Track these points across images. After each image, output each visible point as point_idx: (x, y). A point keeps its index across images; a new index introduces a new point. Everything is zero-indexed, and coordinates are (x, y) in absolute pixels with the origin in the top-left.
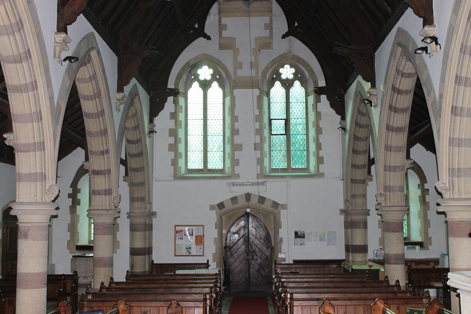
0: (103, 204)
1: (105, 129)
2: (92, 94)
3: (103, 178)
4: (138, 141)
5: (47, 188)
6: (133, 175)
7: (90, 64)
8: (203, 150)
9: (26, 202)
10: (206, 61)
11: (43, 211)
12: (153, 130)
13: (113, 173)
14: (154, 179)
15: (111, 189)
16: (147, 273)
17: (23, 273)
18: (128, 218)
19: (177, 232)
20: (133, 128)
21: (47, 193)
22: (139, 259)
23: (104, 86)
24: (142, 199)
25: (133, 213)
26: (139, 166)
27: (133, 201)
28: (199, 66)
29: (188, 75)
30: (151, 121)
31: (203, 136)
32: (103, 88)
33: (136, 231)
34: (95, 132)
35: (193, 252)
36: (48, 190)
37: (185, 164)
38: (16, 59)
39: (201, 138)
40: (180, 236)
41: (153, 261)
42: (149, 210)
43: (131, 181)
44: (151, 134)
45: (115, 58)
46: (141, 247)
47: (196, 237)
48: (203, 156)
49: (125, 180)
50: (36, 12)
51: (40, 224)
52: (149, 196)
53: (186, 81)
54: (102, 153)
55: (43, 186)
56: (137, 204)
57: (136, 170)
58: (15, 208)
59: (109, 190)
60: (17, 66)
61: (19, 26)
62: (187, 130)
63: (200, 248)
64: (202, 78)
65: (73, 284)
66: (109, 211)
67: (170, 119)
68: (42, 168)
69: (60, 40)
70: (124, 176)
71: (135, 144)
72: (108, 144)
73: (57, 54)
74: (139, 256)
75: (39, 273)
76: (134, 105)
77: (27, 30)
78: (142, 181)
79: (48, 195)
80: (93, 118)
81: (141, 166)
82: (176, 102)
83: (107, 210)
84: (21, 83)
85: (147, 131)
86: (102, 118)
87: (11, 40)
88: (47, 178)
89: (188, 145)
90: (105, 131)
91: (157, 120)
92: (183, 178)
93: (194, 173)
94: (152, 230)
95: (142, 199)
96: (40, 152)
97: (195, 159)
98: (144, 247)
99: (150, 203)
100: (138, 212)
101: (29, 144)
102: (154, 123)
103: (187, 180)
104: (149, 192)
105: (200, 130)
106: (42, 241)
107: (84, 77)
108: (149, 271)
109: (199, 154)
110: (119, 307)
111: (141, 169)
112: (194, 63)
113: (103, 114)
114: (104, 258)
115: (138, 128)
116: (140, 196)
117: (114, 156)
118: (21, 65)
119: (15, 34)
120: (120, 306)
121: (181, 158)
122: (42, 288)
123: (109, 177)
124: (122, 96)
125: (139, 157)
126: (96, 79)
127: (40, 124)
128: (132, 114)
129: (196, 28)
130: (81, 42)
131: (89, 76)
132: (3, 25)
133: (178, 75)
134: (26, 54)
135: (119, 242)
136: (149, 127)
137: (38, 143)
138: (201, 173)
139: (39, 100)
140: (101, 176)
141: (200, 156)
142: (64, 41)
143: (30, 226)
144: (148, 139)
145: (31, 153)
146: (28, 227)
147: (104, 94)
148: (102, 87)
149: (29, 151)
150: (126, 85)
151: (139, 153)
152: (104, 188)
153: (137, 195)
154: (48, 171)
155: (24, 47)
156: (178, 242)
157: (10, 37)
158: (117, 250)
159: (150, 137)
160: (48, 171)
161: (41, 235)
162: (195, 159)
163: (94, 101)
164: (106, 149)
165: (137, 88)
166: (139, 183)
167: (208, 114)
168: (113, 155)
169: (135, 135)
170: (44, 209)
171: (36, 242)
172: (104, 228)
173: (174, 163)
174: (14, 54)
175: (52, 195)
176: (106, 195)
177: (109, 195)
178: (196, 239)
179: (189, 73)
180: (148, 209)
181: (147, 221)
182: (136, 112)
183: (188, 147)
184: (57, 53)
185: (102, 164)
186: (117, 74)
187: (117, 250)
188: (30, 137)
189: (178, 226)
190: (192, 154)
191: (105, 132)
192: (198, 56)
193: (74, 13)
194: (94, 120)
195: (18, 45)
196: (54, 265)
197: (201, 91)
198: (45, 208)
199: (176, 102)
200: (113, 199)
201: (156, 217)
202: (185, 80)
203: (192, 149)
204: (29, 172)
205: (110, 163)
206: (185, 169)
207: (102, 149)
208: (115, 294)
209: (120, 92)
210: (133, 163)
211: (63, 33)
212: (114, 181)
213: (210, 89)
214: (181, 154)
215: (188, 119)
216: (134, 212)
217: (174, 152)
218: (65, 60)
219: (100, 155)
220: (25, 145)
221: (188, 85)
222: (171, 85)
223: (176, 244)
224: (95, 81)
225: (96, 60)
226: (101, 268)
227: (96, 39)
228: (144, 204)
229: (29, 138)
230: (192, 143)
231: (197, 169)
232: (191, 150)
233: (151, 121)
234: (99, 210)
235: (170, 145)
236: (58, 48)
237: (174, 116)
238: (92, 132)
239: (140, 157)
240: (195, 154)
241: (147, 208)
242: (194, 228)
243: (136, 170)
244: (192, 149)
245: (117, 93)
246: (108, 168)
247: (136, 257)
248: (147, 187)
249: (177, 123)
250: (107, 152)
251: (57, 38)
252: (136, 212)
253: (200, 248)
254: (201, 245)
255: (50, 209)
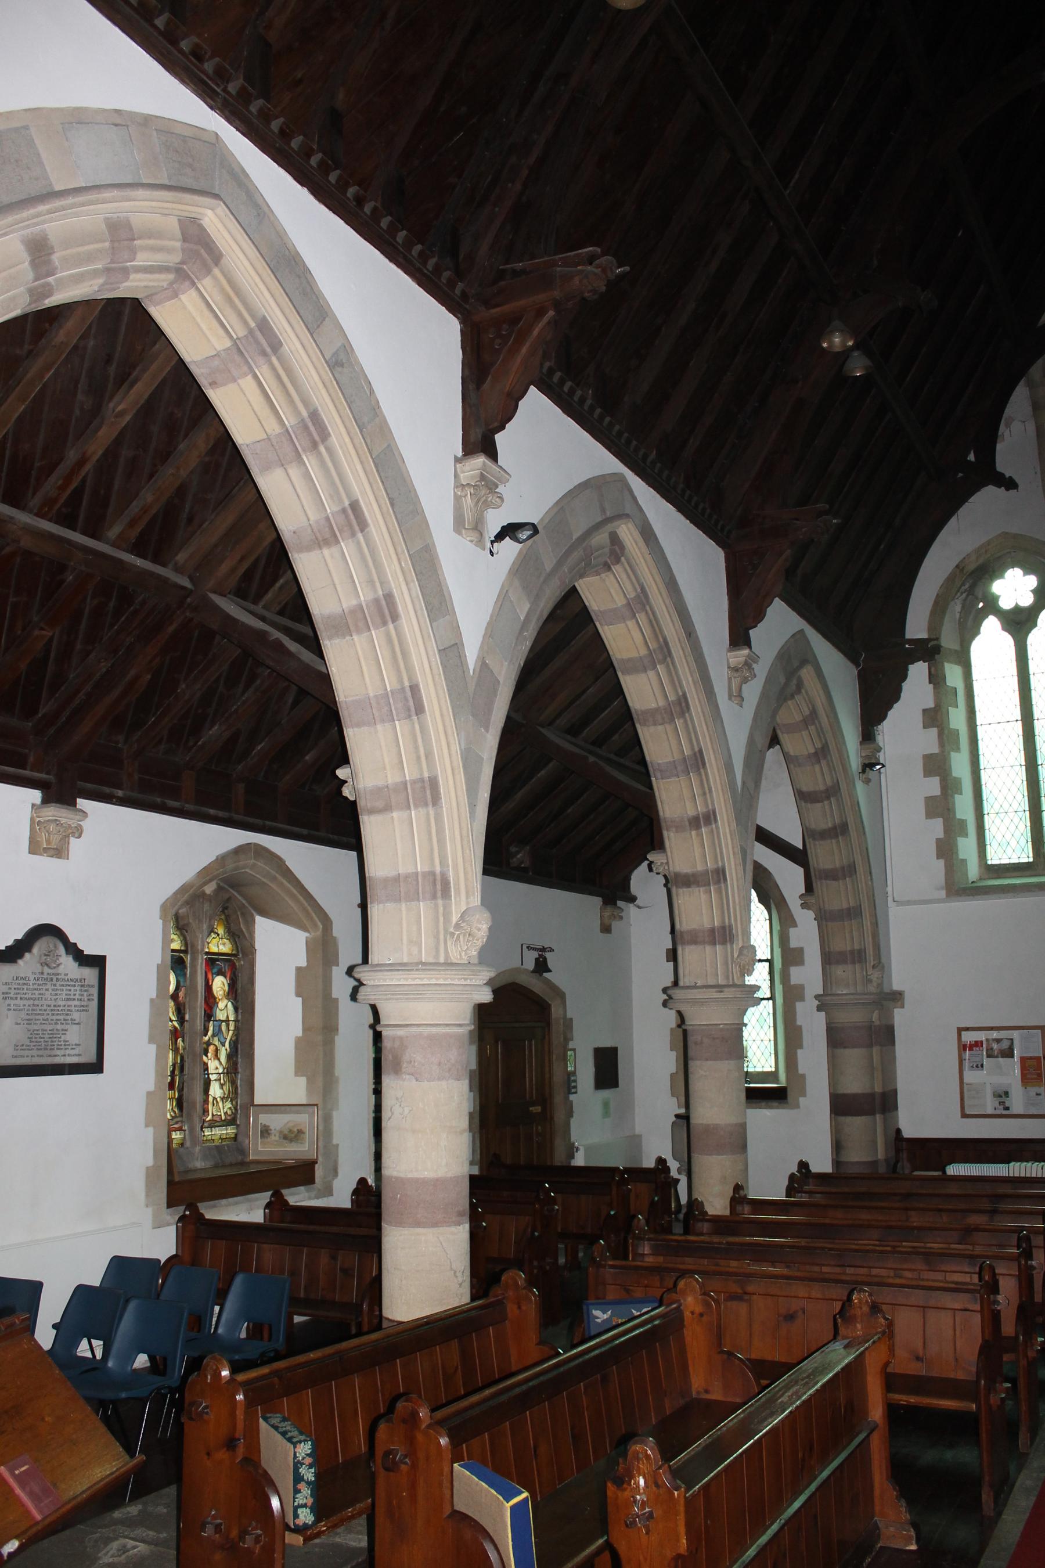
0: (708, 969)
1: (695, 754)
2: (643, 652)
3: (702, 893)
4: (832, 792)
5: (455, 919)
6: (825, 890)
7: (622, 564)
8: (1027, 809)
9: (390, 962)
10: (1013, 554)
11: (438, 988)
12: (873, 761)
13: (732, 879)
14: (890, 899)
15: (730, 927)
16: (882, 1169)
17: (392, 1177)
18: (819, 1009)
19: (964, 1047)
20: (809, 756)
21: (452, 934)
22: (855, 1124)
23: (677, 627)
24: (857, 957)
25: (830, 995)
26: (838, 865)
27: (830, 964)
28: (994, 571)
29: (965, 600)
30: (868, 736)
31: (1024, 768)
32: (674, 633)
33: (845, 1047)
34: (667, 763)
35: (1017, 1105)
36: (457, 926)
37: (979, 852)
38: (318, 535)
39: (1020, 774)
40: (974, 1059)
41: (898, 1131)
42: (880, 985)
43: (822, 907)
44: (871, 774)
45: (717, 556)
46: (860, 1091)
47: (1023, 1060)
48: (1028, 824)
49: (804, 906)
50: (372, 391)
51: (434, 1030)
52: (877, 947)
53: (960, 619)
54: (695, 823)
55: (437, 912)
56: (839, 971)
57: (832, 875)
58: (372, 983)
59: (724, 928)
60: (324, 557)
61: (310, 434)
62: (978, 755)
63: (1037, 1094)
64: (1006, 604)
65: (656, 1196)
66: (726, 990)
67: (924, 727)
68: (432, 860)
69: (472, 477)
70: (802, 895)
71: (822, 802)
72: (708, 795)
73: (468, 519)
74: (855, 1118)
75: (437, 1180)
76: (803, 691)
77: (341, 447)
78: (852, 904)
79: (458, 939)
80: (655, 724)
81: (845, 862)
82: (936, 679)
83: (720, 988)
84: (345, 606)
85: (855, 762)
86: (681, 721)
87: (294, 479)
88: (452, 890)
89: (984, 798)
90: (696, 760)
91: (888, 731)
92: (975, 891)
93: (1008, 874)
94: (892, 1041)
95: (857, 957)
96: (422, 811)
97: (1008, 836)
98: (868, 1091)
99: (881, 964)
100: (844, 992)
101: (387, 787)
102: (879, 739)
103: (986, 896)
104: (875, 935)
105: (1016, 752)
106: (444, 1083)
107: (612, 606)
108: (886, 1160)
109: (1016, 820)
110: (682, 1301)
111: (848, 871)
112: (978, 564)
113: (685, 709)
114: (716, 1127)
115: (825, 758)
116: (849, 948)
117: (730, 831)
118: (334, 550)
119: (302, 459)
120: (685, 1300)
121: (966, 835)
122: (449, 1226)
123: (719, 891)
124: (744, 658)
125: (837, 837)
126: (648, 608)
127: (417, 727)
128: (802, 718)
129: (970, 461)
130: (572, 494)
131: (624, 602)
132: (265, 436)
133: (936, 603)
134: (347, 517)
135: (803, 1076)
136: (863, 755)
137: (414, 782)
138: (1028, 873)
139: (405, 654)
140: (697, 889)
141: (1022, 827)
142: (482, 477)
143: (407, 1037)
144: (860, 787)
145: (395, 814)
146: (401, 1038)
147: (681, 651)
148: (672, 630)
149: (387, 808)
150: (756, 626)
151: (834, 828)
152: (707, 925)
153: (839, 945)
154: (455, 866)
155: (335, 495)
156: (970, 1076)
157: (290, 471)
158: (801, 1099)
159: (867, 781)
160: (455, 866)
161: (439, 1064)
162: (1008, 836)
163: (651, 674)
164: (705, 810)
165: (808, 642)
166: (843, 910)
167: (1034, 702)
168: (729, 826)
169: (819, 776)
170: (441, 982)
171: (425, 1084)
172: (714, 1039)
173: (946, 849)
174: (309, 520)
175: (468, 941)
176: (713, 943)
177: (724, 942)
178: (1023, 1068)
179: (968, 596)
180: (875, 984)
181: (875, 1016)
182: (814, 713)
183: (985, 802)
184: (468, 515)
185: (697, 854)
186: (726, 597)
187: (801, 1099)
188: (388, 767)
189: (967, 1029)
190: (998, 821)
191: (697, 762)
192: (989, 543)
193: (509, 394)
194: (660, 728)
195: (318, 491)
196: (640, 1136)
197: (1007, 641)
198: (446, 979)
199: (936, 679)
200: (738, 956)
201: (902, 1007)
202: (958, 616)
203: (996, 807)
204: (392, 873)
205: (721, 849)
206: (980, 866)
207: (691, 812)
208: (716, 1243)
209: (737, 648)
210: (823, 856)
211: (478, 456)
212: (737, 901)
213: (1034, 631)
214: (963, 823)
215: (978, 722)
216: (834, 992)
217: (941, 820)
218: (499, 537)
219: (688, 828)
220: (378, 791)
221: (969, 630)
222: (916, 627)
223: (965, 1081)
224: (647, 613)
225: (639, 555)
226: (710, 1157)
227: (636, 494)
228: (862, 970)
229: (385, 768)
230: (995, 792)
231: (1014, 864)
232: (992, 811)
233: (868, 736)
234: (695, 987)
235: (929, 801)
236: (468, 502)
237: (934, 717)
238: (659, 764)
239: (840, 838)
240: (1007, 821)
241: (870, 981)
242: (1015, 1034)
243: (832, 875)
244: (996, 807)
245: (730, 650)
246: (715, 866)
247: (849, 1120)
248: (867, 923)
249: (947, 738)
250: (710, 817)
251: (463, 472)
252: (840, 992)
253: (1037, 1094)
254: (1040, 1086)
255: (463, 982)
